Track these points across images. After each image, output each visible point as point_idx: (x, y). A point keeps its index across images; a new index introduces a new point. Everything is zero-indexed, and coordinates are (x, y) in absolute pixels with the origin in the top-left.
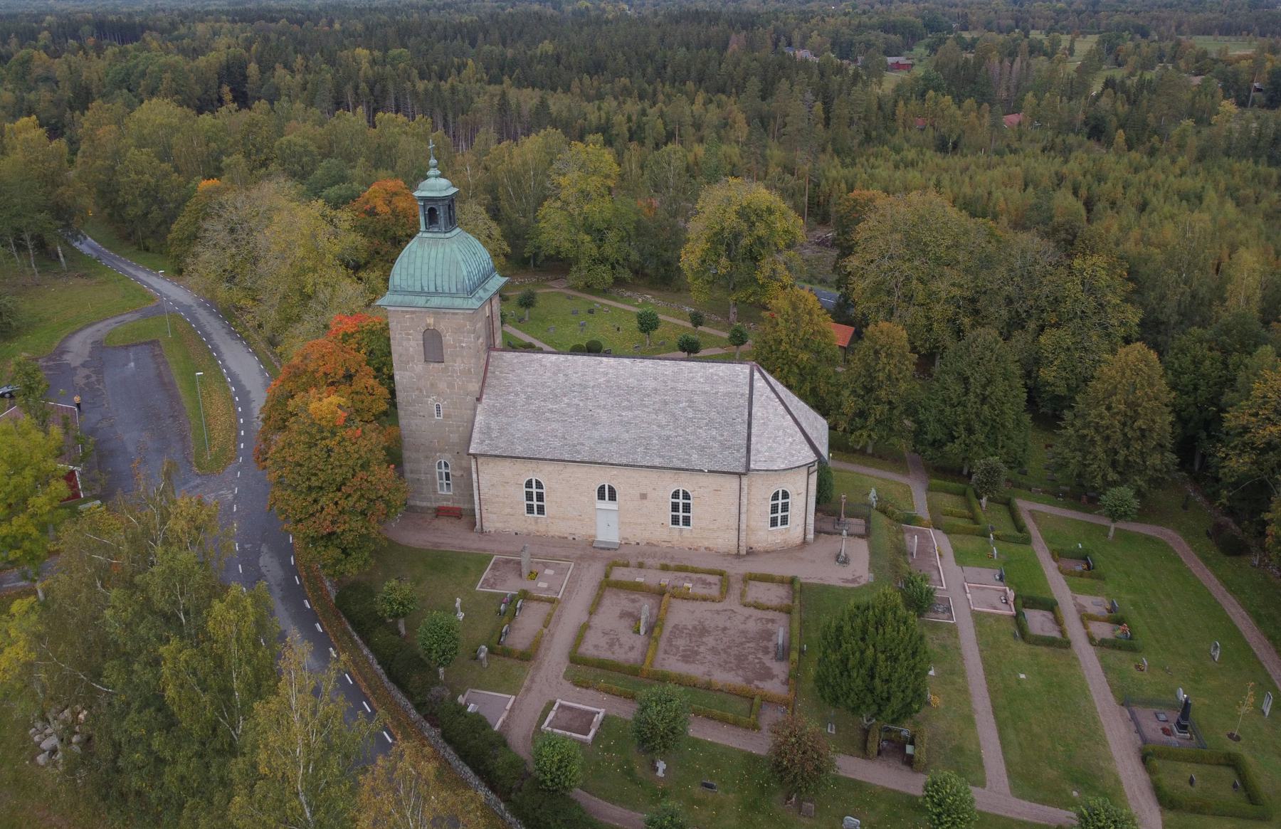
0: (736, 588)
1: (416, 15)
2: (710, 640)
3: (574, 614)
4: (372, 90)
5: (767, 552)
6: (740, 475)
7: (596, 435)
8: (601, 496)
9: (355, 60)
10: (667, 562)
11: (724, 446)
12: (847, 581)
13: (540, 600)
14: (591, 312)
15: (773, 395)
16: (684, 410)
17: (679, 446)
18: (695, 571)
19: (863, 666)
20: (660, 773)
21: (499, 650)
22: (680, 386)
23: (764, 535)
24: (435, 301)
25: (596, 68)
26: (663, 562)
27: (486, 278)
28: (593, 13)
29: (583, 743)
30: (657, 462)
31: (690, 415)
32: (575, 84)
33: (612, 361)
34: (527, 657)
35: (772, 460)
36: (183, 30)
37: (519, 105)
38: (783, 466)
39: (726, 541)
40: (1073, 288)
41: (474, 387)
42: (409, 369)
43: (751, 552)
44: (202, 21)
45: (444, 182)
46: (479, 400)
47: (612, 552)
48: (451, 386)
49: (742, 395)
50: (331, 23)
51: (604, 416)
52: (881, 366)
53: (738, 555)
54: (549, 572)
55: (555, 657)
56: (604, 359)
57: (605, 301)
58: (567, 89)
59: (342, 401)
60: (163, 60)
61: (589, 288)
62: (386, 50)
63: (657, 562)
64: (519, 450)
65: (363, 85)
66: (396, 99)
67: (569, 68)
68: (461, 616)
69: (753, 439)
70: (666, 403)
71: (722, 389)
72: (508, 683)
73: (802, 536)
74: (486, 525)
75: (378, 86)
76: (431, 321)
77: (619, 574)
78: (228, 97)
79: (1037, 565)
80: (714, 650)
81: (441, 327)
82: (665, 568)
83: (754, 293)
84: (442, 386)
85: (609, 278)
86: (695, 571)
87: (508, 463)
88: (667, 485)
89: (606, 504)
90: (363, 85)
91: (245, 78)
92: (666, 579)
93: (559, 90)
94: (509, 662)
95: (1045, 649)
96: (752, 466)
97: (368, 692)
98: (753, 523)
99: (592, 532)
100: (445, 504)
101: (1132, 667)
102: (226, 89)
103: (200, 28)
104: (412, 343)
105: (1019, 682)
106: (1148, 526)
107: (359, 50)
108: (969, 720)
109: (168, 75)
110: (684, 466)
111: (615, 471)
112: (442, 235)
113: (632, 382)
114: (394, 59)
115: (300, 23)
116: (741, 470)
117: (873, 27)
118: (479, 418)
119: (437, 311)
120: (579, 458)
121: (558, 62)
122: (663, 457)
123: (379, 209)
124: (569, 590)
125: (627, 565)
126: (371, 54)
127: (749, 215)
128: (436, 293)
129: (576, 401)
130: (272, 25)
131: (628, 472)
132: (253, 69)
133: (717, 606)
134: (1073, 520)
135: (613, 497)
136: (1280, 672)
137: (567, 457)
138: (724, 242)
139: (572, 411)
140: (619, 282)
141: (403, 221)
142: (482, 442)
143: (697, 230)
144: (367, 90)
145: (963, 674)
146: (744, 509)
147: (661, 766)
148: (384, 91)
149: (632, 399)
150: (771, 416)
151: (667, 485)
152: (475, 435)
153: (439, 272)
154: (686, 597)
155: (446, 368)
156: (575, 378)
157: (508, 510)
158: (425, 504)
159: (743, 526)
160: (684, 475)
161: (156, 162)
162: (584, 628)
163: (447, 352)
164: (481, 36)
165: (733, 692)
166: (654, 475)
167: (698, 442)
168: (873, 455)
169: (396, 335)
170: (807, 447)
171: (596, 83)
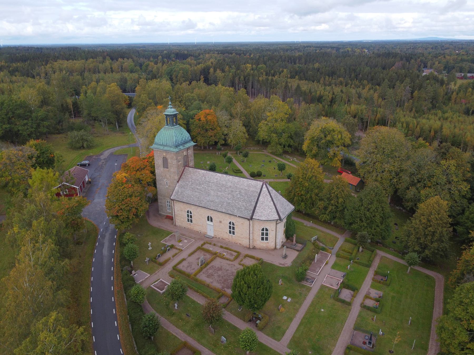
0: (241, 258)
1: (282, 52)
2: (220, 273)
3: (184, 255)
4: (245, 79)
5: (260, 249)
6: (248, 219)
7: (208, 199)
8: (208, 220)
9: (246, 68)
10: (223, 245)
11: (246, 209)
12: (281, 264)
13: (176, 249)
14: (270, 162)
15: (268, 194)
16: (237, 194)
17: (232, 206)
18: (230, 250)
19: (255, 289)
20: (176, 308)
21: (154, 260)
22: (238, 186)
23: (259, 243)
24: (166, 148)
25: (332, 74)
26: (222, 245)
27: (186, 142)
28: (350, 53)
29: (160, 293)
30: (224, 211)
31: (239, 196)
32: (322, 80)
33: (220, 175)
34: (162, 265)
35: (261, 216)
36: (201, 56)
37: (291, 86)
38: (264, 219)
39: (245, 242)
40: (438, 172)
41: (177, 178)
42: (159, 170)
43: (254, 248)
44: (209, 53)
45: (173, 110)
46: (178, 182)
47: (209, 239)
48: (170, 176)
50: (251, 54)
51: (212, 192)
52: (334, 191)
53: (249, 248)
54: (186, 241)
55: (169, 267)
56: (218, 174)
57: (279, 159)
58: (319, 81)
59: (127, 175)
60: (181, 66)
61: (273, 153)
62: (258, 65)
63: (219, 244)
64: (184, 200)
65: (242, 77)
66: (252, 83)
67: (321, 73)
68: (150, 248)
69: (257, 208)
70: (232, 191)
71: (251, 189)
72: (151, 272)
74: (176, 223)
75: (247, 78)
76: (164, 154)
77: (206, 247)
78: (202, 79)
79: (365, 276)
80: (219, 276)
81: (167, 157)
82: (221, 247)
83: (327, 161)
84: (168, 176)
85: (281, 151)
86: (230, 250)
87: (182, 203)
88: (227, 220)
89: (209, 223)
90: (242, 77)
91: (209, 73)
92: (218, 250)
93: (315, 81)
94: (155, 265)
95: (340, 304)
96: (254, 217)
97: (115, 265)
98: (255, 238)
99: (206, 231)
100: (169, 215)
101: (370, 318)
102: (202, 77)
103: (207, 55)
105: (320, 311)
106: (434, 273)
107: (248, 65)
108: (291, 319)
109: (181, 72)
110: (231, 213)
111: (212, 212)
113: (224, 183)
114: (260, 68)
115: (240, 55)
116: (249, 218)
117: (467, 61)
118: (176, 188)
119: (166, 151)
120: (201, 205)
121: (318, 71)
122: (226, 209)
123: (202, 119)
124: (187, 248)
125: (210, 244)
126: (252, 66)
127: (326, 132)
128: (166, 146)
129: (206, 187)
130: (230, 55)
131: (216, 213)
132: (212, 70)
133: (231, 263)
134: (395, 262)
135: (212, 221)
137: (197, 204)
138: (315, 141)
139: (203, 189)
140: (285, 152)
141: (209, 123)
142: (175, 195)
143: (308, 135)
144: (243, 79)
145: (301, 305)
146: (251, 232)
147: (176, 305)
148: (248, 79)
149: (223, 188)
150: (265, 201)
151: (227, 220)
152: (174, 193)
154: (223, 258)
155: (169, 170)
156: (207, 179)
157: (182, 219)
158: (163, 214)
159: (251, 238)
160: (232, 217)
161: (148, 99)
162: (184, 260)
163: (169, 165)
164: (298, 60)
165: (215, 290)
166: (223, 215)
167: (238, 206)
168: (332, 225)
169: (156, 158)
170: (276, 214)
171: (330, 79)
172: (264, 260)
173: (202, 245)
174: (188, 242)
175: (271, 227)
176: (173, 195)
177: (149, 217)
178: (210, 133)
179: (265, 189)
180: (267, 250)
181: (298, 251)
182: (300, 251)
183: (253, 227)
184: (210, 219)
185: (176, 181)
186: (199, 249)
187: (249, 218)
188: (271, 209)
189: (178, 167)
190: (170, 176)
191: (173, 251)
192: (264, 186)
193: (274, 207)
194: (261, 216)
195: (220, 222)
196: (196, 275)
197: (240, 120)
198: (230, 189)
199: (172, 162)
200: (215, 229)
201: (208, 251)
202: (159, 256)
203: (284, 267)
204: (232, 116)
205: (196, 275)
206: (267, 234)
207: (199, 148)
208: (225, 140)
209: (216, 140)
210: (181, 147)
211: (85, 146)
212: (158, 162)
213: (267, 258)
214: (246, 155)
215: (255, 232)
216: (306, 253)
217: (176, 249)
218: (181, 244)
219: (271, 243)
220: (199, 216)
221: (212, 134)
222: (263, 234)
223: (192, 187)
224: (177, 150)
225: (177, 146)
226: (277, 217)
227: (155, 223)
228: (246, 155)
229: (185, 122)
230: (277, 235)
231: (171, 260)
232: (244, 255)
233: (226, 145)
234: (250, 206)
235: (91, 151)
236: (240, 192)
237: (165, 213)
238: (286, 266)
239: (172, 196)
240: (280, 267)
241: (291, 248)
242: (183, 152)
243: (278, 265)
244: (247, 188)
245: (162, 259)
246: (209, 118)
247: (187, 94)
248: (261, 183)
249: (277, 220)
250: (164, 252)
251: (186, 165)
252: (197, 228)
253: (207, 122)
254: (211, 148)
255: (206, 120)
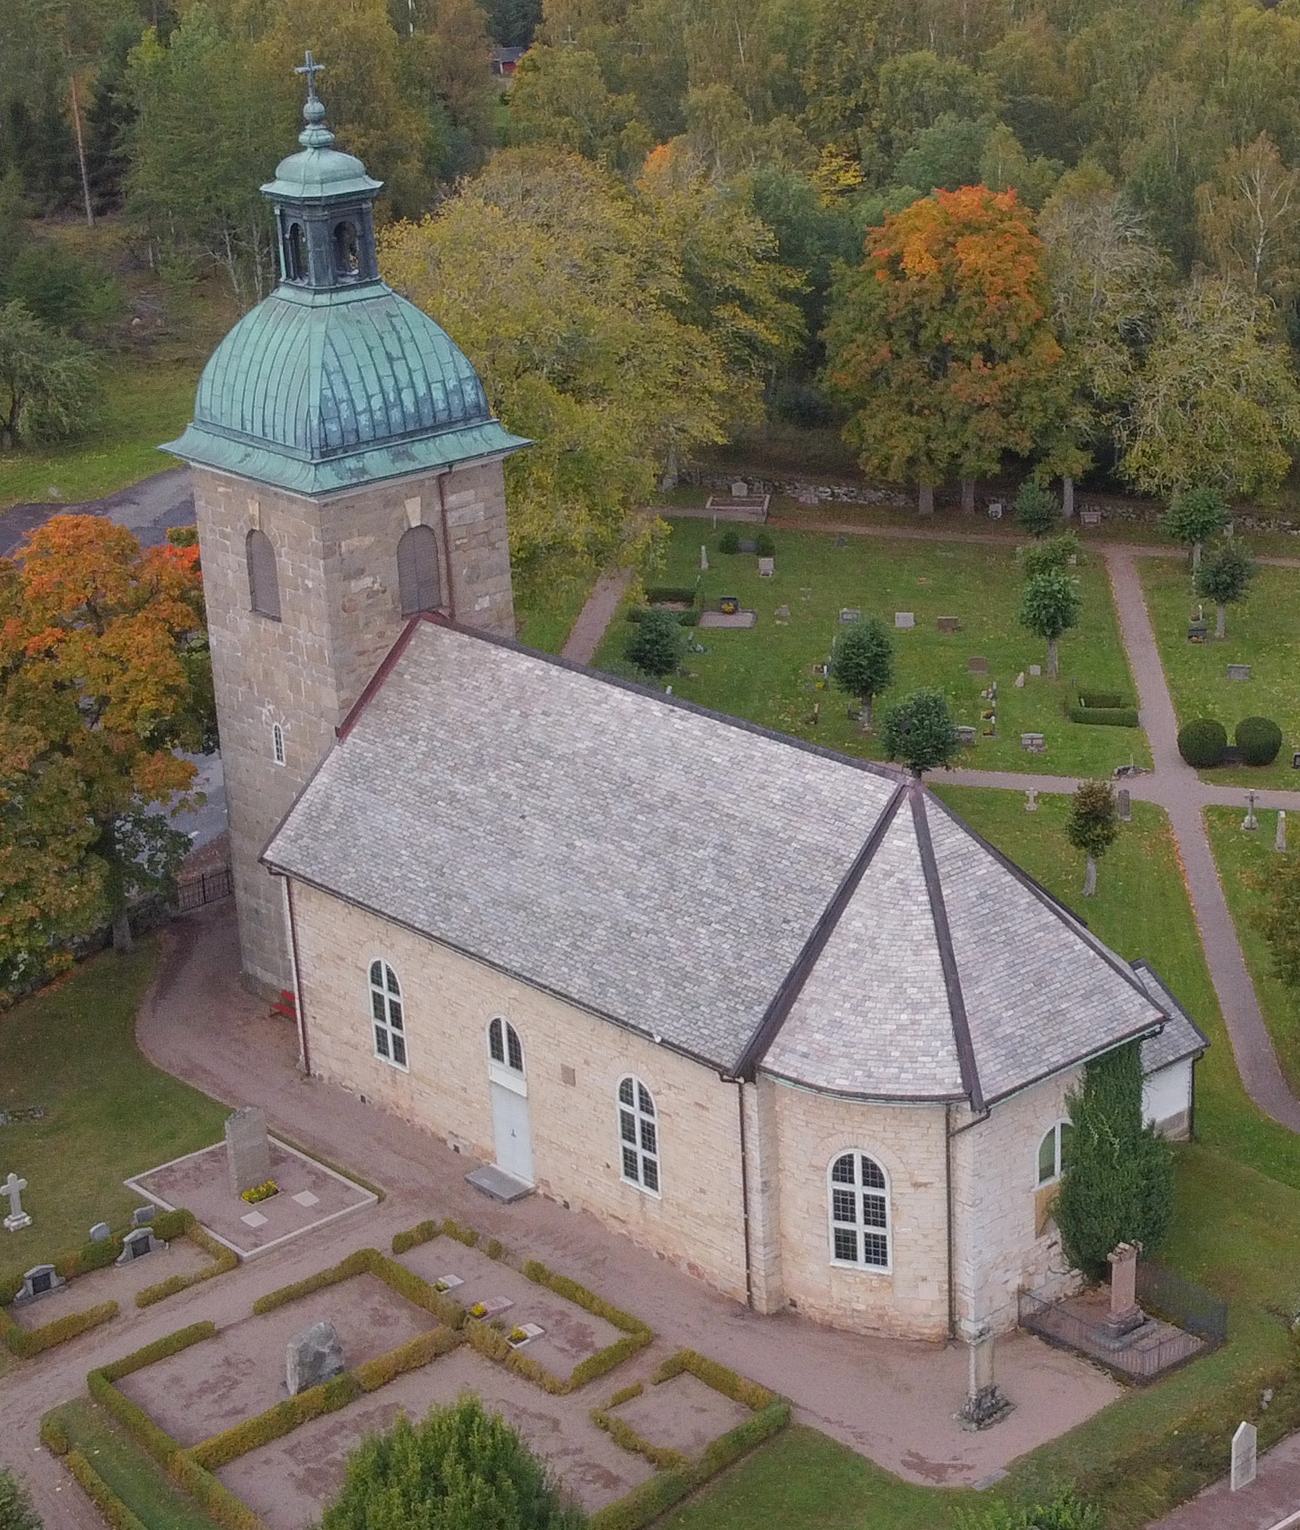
0: (636, 1373)
5: (829, 1328)
8: (497, 1054)
12: (919, 1464)
13: (205, 1246)
15: (919, 881)
16: (699, 867)
22: (725, 799)
31: (706, 884)
35: (824, 1056)
38: (842, 1083)
39: (720, 1258)
41: (331, 700)
42: (231, 634)
43: (786, 1314)
45: (334, 160)
46: (342, 733)
48: (295, 686)
49: (839, 860)
54: (307, 1199)
56: (617, 693)
69: (810, 989)
70: (673, 838)
73: (940, 1314)
74: (314, 1056)
88: (612, 1059)
89: (500, 1073)
96: (768, 1061)
98: (793, 1232)
99: (486, 1143)
104: (231, 557)
110: (621, 1012)
112: (307, 298)
113: (638, 765)
118: (322, 778)
120: (441, 928)
122: (592, 974)
123: (908, 263)
124: (285, 1251)
128: (262, 442)
129: (509, 786)
136: (287, 1493)
137: (421, 919)
146: (755, 1182)
150: (883, 940)
152: (295, 818)
153: (272, 392)
157: (347, 1032)
158: (268, 978)
159: (758, 1231)
162: (203, 1334)
163: (286, 593)
169: (206, 533)
170: (947, 1050)
172: (803, 1419)
173: (403, 1243)
174: (319, 1211)
175: (908, 1155)
176: (288, 830)
177: (161, 994)
178: (966, 384)
179: (901, 840)
180: (872, 1346)
181: (1121, 1377)
182: (1145, 1381)
183: (772, 1140)
184: (505, 1045)
185: (327, 727)
186: (361, 1265)
187: (729, 1060)
188: (915, 1007)
189: (344, 616)
190: (295, 686)
191: (182, 1261)
192: (904, 814)
193: (941, 993)
194: (824, 1056)
195: (569, 1076)
196: (217, 1458)
197: (1264, 291)
198: (666, 820)
199: (302, 571)
200: (530, 1124)
201: (416, 1293)
202: (41, 1284)
203: (925, 1492)
204: (1186, 255)
205: (217, 1458)
206: (876, 1212)
207: (901, 501)
208: (1106, 454)
209: (1010, 442)
210: (377, 462)
211: (23, 424)
212: (224, 570)
213: (829, 1401)
214: (1224, 585)
215: (788, 1186)
216: (1169, 1413)
217: (205, 1246)
218: (254, 1219)
219: (907, 1290)
220: (448, 1003)
221: (986, 393)
222: (843, 1206)
223: (425, 780)
224: (329, 478)
225: (327, 453)
226: (948, 1078)
227: (1155, 1133)
228: (1224, 585)
229: (795, 281)
230: (979, 1230)
231: (114, 1327)
232: (672, 1353)
233: (1103, 481)
234: (759, 965)
235: (56, 468)
236: (725, 849)
237: (275, 972)
238: (955, 1481)
239: (279, 841)
240: (903, 1487)
241: (1083, 1355)
242: (392, 502)
243: (894, 1467)
244: (775, 822)
245: (50, 1311)
246: (973, 255)
247: (903, 62)
248: (889, 787)
249: (947, 1101)
250: (103, 1258)
251: (428, 600)
252: (436, 1113)
253: (950, 297)
254: (996, 508)
255: (945, 271)
